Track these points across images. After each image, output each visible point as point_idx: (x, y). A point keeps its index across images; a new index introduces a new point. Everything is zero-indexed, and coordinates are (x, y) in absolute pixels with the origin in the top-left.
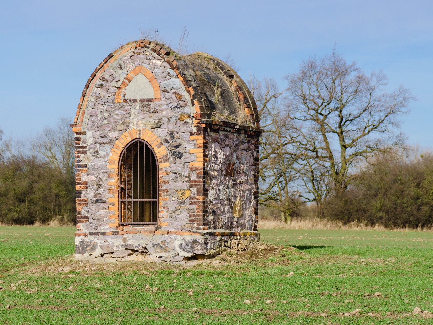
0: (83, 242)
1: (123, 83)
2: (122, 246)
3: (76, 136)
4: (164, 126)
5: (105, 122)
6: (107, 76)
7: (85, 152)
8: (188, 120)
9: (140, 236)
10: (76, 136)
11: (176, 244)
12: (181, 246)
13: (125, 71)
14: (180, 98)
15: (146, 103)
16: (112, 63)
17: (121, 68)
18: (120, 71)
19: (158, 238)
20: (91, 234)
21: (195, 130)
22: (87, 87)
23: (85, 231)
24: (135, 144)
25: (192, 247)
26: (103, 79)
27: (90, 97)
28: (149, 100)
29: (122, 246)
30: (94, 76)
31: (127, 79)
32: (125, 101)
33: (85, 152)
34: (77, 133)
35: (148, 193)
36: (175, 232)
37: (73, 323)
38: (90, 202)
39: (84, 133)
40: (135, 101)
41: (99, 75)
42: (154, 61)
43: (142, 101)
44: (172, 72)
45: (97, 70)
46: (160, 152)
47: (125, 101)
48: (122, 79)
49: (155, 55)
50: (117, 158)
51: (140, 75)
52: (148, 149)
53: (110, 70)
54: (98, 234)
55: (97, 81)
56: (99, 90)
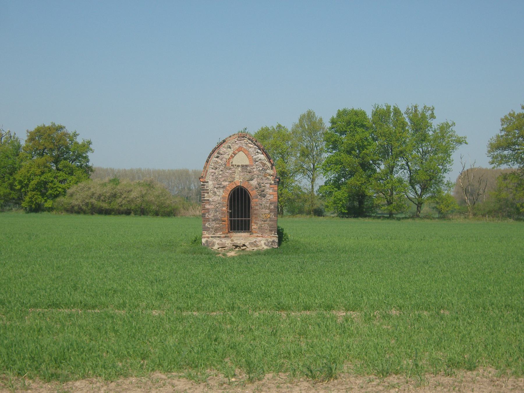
0: (207, 241)
1: (231, 156)
2: (231, 243)
3: (202, 183)
4: (255, 179)
5: (220, 176)
6: (221, 152)
7: (208, 193)
8: (269, 177)
9: (240, 238)
10: (202, 183)
11: (263, 242)
12: (265, 243)
13: (232, 149)
14: (264, 165)
15: (244, 167)
16: (225, 145)
17: (230, 148)
18: (229, 149)
19: (253, 240)
20: (212, 237)
21: (273, 182)
22: (209, 157)
23: (207, 235)
24: (238, 189)
25: (272, 244)
26: (219, 153)
27: (212, 164)
28: (247, 166)
29: (231, 243)
30: (213, 151)
31: (233, 153)
32: (232, 165)
33: (208, 193)
34: (203, 182)
35: (234, 223)
36: (259, 239)
37: (56, 392)
38: (210, 220)
39: (207, 182)
40: (238, 166)
41: (217, 151)
42: (249, 145)
43: (243, 166)
44: (259, 151)
45: (216, 149)
46: (253, 193)
47: (232, 165)
48: (231, 154)
49: (250, 142)
50: (227, 196)
51: (241, 152)
52: (245, 192)
53: (222, 150)
54: (216, 237)
55: (216, 154)
56: (217, 159)
